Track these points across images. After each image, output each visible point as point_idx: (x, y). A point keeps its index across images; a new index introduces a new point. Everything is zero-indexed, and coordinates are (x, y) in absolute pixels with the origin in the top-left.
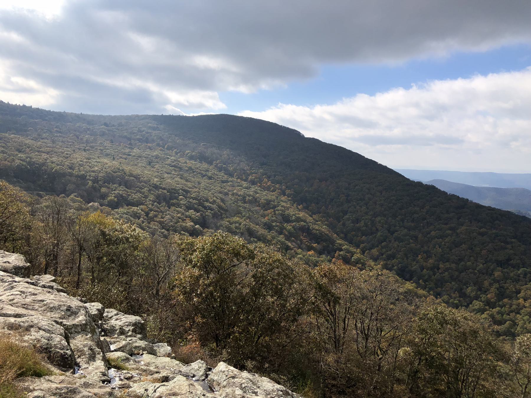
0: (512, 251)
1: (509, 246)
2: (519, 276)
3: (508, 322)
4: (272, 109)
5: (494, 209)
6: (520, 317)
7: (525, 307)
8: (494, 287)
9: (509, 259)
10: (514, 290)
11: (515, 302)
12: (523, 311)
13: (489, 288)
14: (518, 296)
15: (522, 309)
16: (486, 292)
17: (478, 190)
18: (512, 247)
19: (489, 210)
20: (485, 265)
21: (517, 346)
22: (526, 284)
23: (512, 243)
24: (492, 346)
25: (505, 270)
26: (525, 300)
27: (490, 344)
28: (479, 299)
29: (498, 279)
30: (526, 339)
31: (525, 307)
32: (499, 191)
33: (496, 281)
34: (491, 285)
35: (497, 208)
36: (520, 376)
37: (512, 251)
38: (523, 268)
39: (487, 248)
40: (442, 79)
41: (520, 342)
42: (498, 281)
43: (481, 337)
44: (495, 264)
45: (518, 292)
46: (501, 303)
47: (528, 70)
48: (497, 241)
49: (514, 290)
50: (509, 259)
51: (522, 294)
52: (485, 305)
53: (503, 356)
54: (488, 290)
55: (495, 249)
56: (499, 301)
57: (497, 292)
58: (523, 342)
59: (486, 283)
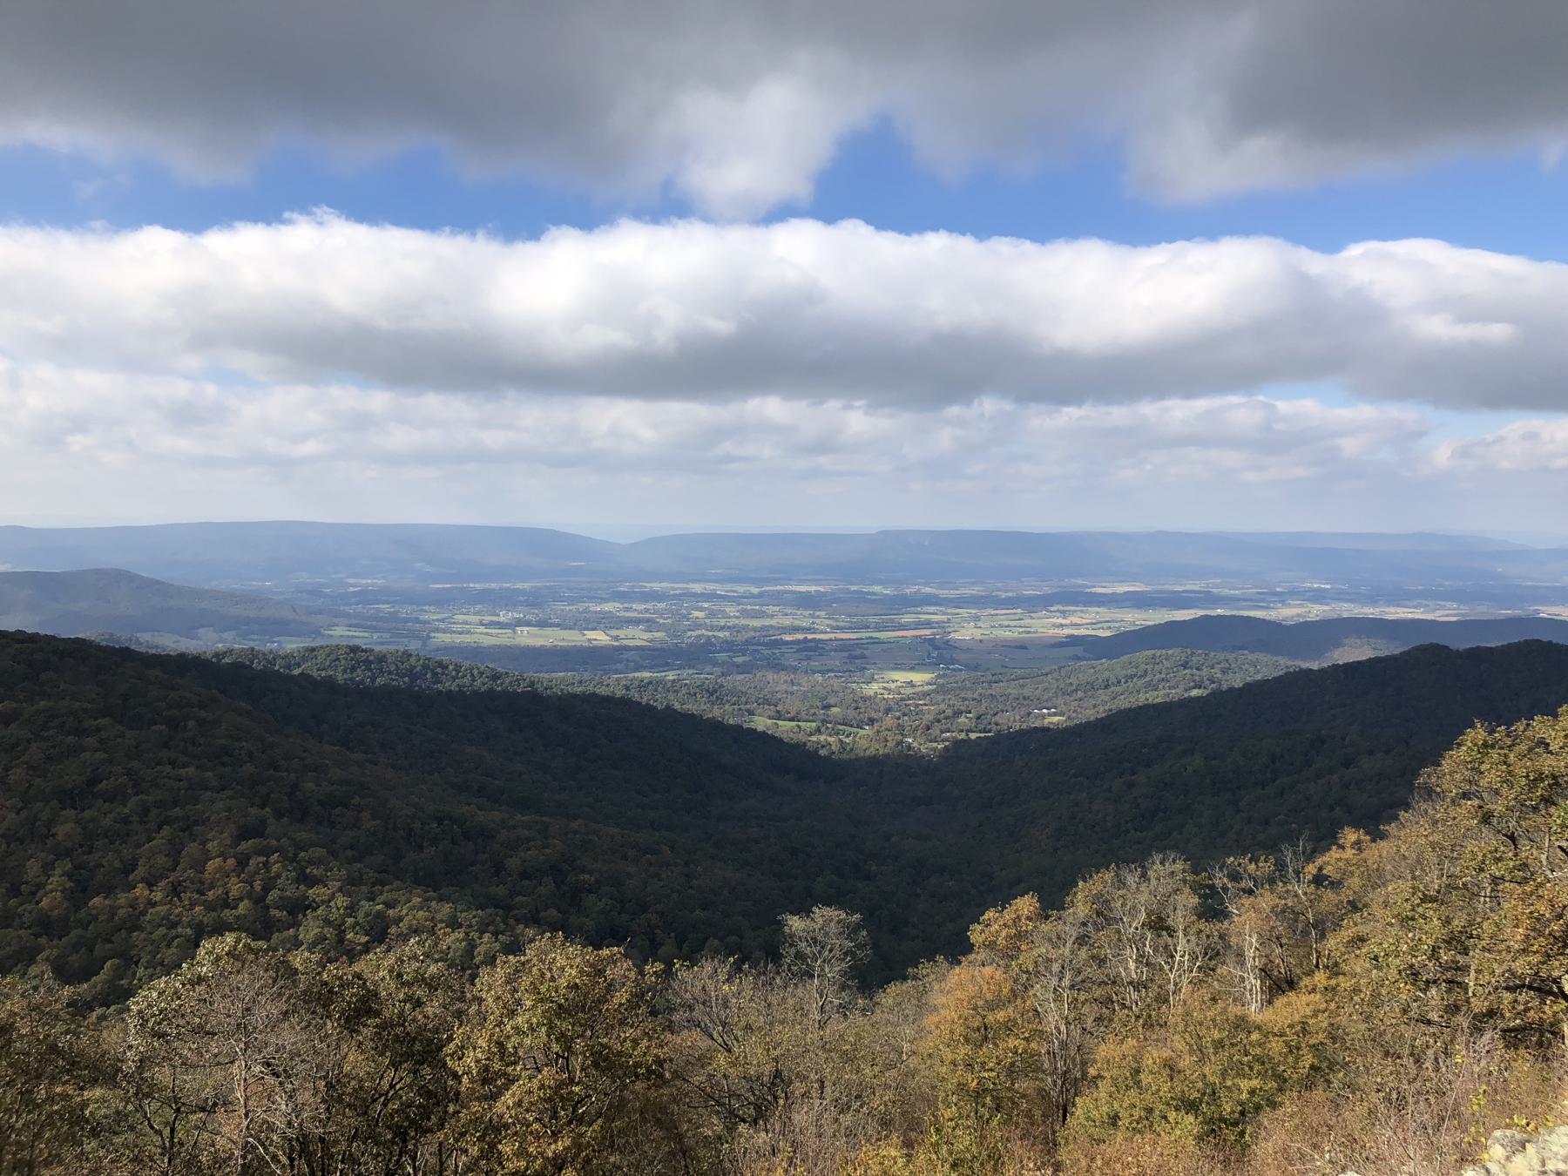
0: (101, 755)
1: (90, 741)
2: (126, 821)
3: (108, 964)
4: (93, 231)
5: (34, 638)
6: (143, 936)
7: (154, 905)
8: (58, 871)
9: (93, 782)
10: (117, 864)
11: (123, 898)
12: (148, 917)
13: (43, 879)
14: (131, 877)
15: (143, 913)
16: (34, 894)
17: (765, 651)
18: (101, 741)
19: (22, 642)
20: (23, 814)
21: (132, 1022)
22: (150, 839)
23: (98, 730)
24: (60, 1053)
25: (88, 814)
26: (151, 885)
27: (53, 1048)
28: (17, 922)
29: (69, 845)
30: (155, 995)
31: (154, 905)
32: (44, 583)
33: (62, 853)
34: (47, 868)
35: (42, 632)
36: (150, 1106)
37: (101, 755)
38: (136, 794)
39: (25, 758)
40: (348, 218)
41: (140, 1012)
42: (68, 853)
43: (22, 1037)
44: (54, 803)
45: (130, 868)
46: (82, 914)
47: (320, 223)
48: (51, 733)
49: (117, 864)
50: (93, 782)
51: (141, 871)
52: (36, 936)
53: (95, 1067)
54: (40, 886)
55: (49, 758)
56: (77, 909)
57: (70, 884)
58: (150, 1006)
59: (33, 867)
